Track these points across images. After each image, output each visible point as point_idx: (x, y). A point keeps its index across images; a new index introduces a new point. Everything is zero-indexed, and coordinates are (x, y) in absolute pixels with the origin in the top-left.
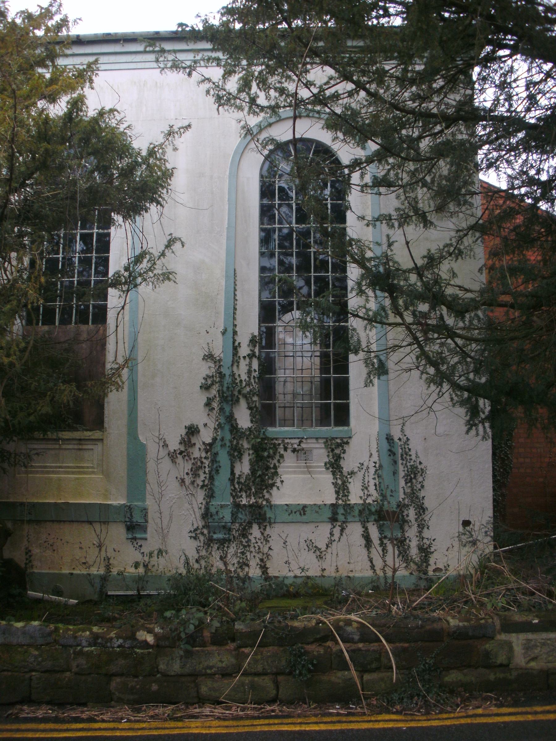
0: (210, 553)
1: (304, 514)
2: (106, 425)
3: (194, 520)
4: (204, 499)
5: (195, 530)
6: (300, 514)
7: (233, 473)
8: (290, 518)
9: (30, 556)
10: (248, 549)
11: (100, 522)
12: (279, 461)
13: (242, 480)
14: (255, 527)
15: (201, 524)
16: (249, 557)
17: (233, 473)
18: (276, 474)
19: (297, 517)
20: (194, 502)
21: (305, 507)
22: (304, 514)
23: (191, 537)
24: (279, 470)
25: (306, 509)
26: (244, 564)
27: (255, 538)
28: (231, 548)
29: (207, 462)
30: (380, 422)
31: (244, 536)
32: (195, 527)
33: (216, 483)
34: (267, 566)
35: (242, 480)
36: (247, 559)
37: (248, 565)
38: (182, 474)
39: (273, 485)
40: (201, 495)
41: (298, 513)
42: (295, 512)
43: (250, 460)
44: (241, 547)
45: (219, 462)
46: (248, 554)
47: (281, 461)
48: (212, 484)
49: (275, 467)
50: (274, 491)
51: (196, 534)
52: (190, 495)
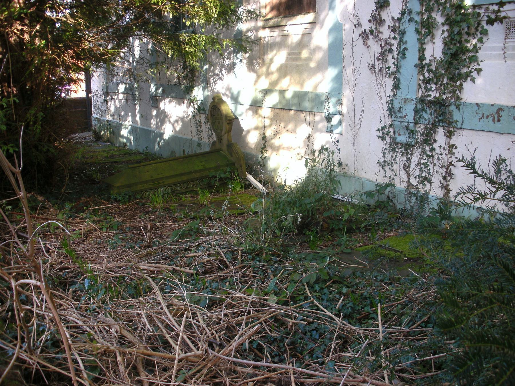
0: (395, 160)
1: (499, 120)
2: (317, 6)
3: (382, 116)
4: (392, 90)
5: (383, 129)
6: (494, 120)
7: (422, 58)
8: (480, 125)
9: (266, 142)
10: (431, 160)
11: (309, 112)
12: (481, 40)
13: (433, 68)
14: (441, 131)
15: (387, 121)
16: (431, 171)
17: (422, 58)
18: (474, 59)
19: (489, 123)
20: (383, 94)
21: (500, 109)
22: (499, 120)
23: (379, 137)
24: (481, 55)
25: (502, 113)
26: (425, 180)
27: (440, 147)
28: (415, 155)
29: (395, 43)
30: (187, 140)
31: (427, 142)
32: (383, 125)
33: (402, 70)
34: (450, 187)
35: (433, 68)
36: (429, 174)
37: (430, 182)
38: (373, 59)
39: (468, 75)
40: (390, 82)
41: (491, 119)
42: (488, 117)
43: (444, 39)
44: (425, 157)
45: (406, 42)
46: (431, 166)
47: (484, 40)
48: (398, 71)
49: (476, 49)
50: (467, 85)
51: (383, 133)
52: (379, 85)
